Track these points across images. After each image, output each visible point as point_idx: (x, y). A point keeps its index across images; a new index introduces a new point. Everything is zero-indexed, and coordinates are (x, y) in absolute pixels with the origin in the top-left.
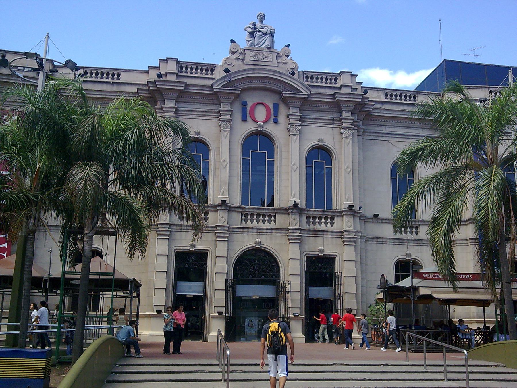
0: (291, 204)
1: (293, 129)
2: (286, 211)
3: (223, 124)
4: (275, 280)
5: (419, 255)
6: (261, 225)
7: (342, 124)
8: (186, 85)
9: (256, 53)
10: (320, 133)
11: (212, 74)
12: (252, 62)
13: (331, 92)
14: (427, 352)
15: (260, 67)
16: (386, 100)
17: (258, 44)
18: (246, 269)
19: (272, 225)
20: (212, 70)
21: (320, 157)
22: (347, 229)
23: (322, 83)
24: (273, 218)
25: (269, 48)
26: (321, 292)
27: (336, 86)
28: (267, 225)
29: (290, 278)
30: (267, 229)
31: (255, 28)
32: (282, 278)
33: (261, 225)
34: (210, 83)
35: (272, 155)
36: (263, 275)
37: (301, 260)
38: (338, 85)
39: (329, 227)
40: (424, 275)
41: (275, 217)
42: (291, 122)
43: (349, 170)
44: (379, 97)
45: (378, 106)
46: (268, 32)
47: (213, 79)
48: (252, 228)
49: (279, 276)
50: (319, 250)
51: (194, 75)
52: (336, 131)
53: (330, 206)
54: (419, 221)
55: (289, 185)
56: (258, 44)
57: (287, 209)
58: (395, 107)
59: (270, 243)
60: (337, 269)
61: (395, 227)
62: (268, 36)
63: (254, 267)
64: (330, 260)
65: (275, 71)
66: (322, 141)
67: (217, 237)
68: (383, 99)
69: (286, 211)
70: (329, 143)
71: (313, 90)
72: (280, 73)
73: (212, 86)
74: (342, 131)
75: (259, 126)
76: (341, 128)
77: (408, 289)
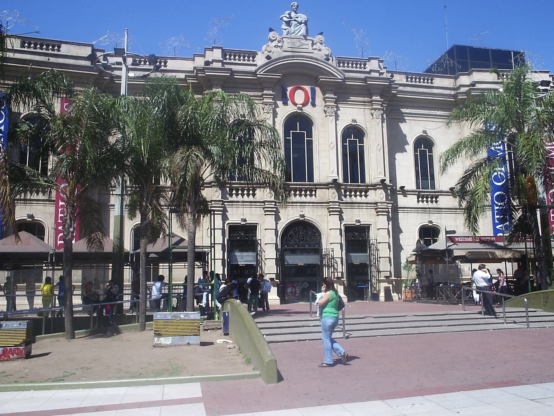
0: (330, 180)
1: (329, 110)
2: (326, 186)
3: (266, 107)
4: (318, 249)
5: (439, 221)
6: (303, 199)
7: (372, 105)
8: (233, 72)
9: (293, 40)
10: (353, 113)
11: (254, 61)
12: (290, 49)
13: (363, 76)
14: (465, 304)
15: (297, 54)
16: (407, 83)
17: (294, 33)
18: (292, 239)
19: (313, 199)
20: (254, 57)
21: (353, 136)
22: (380, 201)
23: (352, 67)
24: (314, 193)
25: (304, 36)
26: (358, 258)
27: (365, 70)
28: (309, 199)
29: (332, 246)
30: (309, 203)
31: (291, 18)
32: (324, 246)
33: (303, 199)
34: (253, 69)
35: (310, 135)
36: (307, 244)
37: (341, 230)
38: (367, 70)
39: (364, 199)
40: (456, 239)
41: (315, 191)
42: (327, 104)
43: (379, 147)
44: (401, 80)
45: (401, 88)
46: (303, 21)
47: (256, 65)
48: (296, 203)
49: (320, 243)
50: (356, 220)
51: (237, 62)
52: (368, 112)
53: (363, 180)
54: (438, 192)
55: (327, 163)
56: (294, 33)
57: (327, 184)
58: (415, 89)
59: (314, 215)
60: (258, 237)
61: (418, 198)
62: (303, 24)
63: (299, 238)
64: (252, 229)
65: (312, 58)
66: (355, 121)
67: (265, 211)
68: (404, 82)
69: (326, 186)
70: (361, 123)
71: (347, 75)
72: (316, 59)
73: (256, 71)
74: (373, 111)
75: (299, 108)
76: (371, 110)
77: (443, 252)
